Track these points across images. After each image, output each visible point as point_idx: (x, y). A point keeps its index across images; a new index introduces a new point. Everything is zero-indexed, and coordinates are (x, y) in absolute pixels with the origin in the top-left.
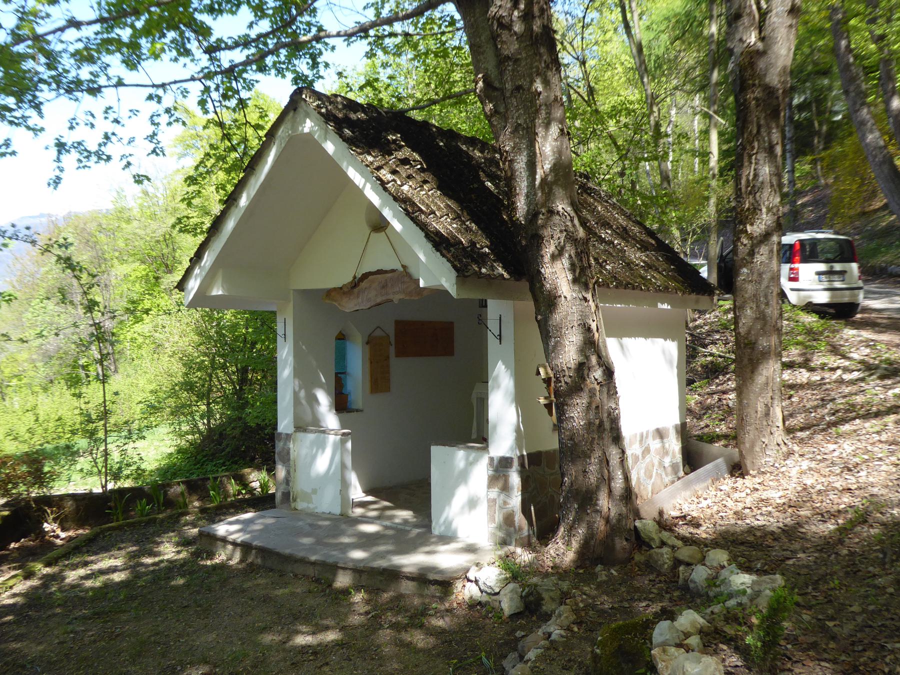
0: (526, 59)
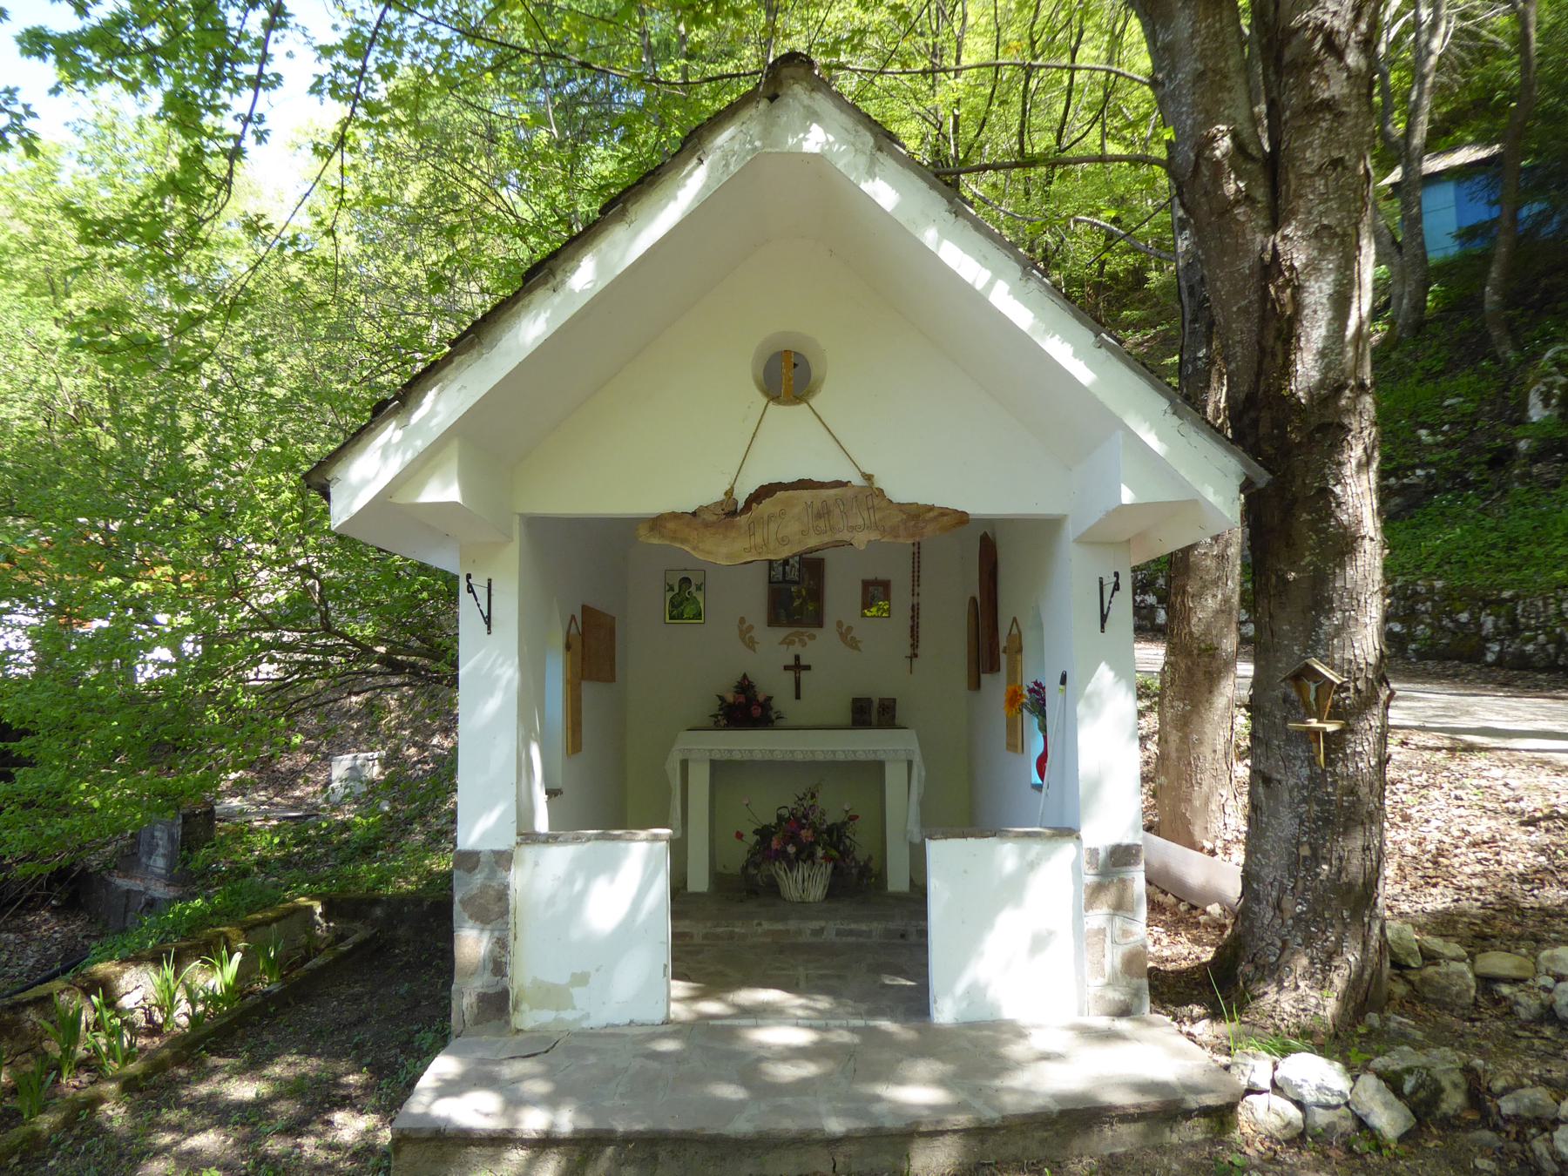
0: (1357, 116)
